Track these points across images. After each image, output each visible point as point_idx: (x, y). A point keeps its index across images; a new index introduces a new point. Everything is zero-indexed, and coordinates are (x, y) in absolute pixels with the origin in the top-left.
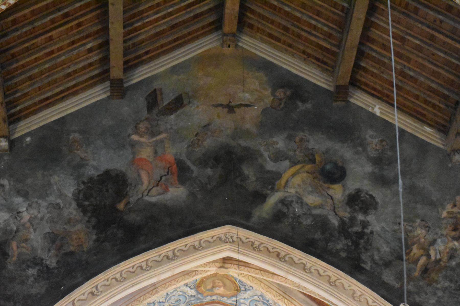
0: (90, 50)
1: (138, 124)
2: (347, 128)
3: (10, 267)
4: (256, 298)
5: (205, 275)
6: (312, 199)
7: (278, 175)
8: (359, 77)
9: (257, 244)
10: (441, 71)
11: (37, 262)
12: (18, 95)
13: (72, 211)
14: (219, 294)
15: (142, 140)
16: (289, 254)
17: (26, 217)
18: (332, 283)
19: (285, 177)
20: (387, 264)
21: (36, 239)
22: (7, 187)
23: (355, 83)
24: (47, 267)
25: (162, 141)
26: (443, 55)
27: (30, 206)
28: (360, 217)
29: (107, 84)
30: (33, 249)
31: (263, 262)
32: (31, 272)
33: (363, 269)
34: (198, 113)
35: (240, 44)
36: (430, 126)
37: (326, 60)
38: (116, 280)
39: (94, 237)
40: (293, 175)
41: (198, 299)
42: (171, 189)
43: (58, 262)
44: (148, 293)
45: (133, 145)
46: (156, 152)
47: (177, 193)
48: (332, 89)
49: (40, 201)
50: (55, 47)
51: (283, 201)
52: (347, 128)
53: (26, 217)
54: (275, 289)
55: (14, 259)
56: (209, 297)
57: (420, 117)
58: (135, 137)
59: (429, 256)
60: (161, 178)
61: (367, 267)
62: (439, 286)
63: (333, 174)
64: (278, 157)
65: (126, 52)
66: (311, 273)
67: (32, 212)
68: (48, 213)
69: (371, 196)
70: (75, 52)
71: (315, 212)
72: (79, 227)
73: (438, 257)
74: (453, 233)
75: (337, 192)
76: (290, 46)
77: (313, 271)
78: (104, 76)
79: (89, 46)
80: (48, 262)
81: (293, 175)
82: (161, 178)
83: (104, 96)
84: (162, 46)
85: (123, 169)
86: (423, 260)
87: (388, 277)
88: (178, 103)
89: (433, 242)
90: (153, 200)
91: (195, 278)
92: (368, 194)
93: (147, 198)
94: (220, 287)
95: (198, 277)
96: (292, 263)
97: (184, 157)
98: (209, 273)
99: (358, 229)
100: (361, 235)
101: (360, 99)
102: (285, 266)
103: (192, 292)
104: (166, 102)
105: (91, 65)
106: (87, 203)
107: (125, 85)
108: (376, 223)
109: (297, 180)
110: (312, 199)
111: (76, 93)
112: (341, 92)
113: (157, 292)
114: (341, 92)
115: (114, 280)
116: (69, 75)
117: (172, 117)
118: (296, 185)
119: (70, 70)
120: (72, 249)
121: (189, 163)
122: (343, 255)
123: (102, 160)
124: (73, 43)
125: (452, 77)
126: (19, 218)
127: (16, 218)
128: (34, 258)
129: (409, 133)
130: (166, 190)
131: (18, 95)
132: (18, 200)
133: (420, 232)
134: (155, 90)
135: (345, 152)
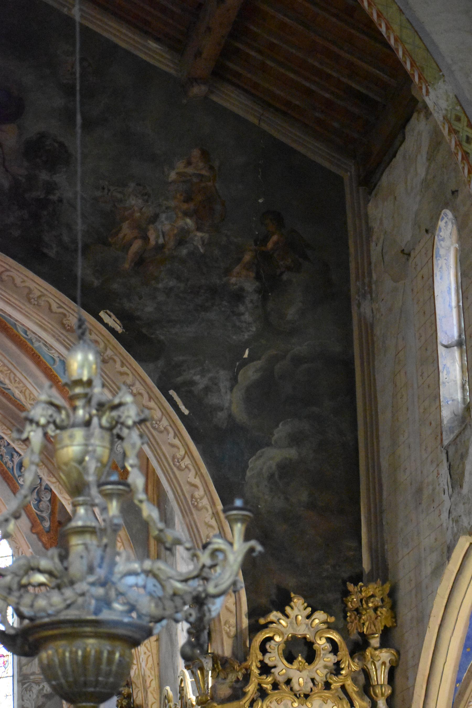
28: (44, 176)
36: (157, 40)
57: (143, 27)
59: (146, 239)
61: (52, 253)
73: (161, 241)
74: (185, 206)
86: (137, 245)
89: (154, 218)
108: (74, 189)
122: (16, 233)
133: (135, 202)
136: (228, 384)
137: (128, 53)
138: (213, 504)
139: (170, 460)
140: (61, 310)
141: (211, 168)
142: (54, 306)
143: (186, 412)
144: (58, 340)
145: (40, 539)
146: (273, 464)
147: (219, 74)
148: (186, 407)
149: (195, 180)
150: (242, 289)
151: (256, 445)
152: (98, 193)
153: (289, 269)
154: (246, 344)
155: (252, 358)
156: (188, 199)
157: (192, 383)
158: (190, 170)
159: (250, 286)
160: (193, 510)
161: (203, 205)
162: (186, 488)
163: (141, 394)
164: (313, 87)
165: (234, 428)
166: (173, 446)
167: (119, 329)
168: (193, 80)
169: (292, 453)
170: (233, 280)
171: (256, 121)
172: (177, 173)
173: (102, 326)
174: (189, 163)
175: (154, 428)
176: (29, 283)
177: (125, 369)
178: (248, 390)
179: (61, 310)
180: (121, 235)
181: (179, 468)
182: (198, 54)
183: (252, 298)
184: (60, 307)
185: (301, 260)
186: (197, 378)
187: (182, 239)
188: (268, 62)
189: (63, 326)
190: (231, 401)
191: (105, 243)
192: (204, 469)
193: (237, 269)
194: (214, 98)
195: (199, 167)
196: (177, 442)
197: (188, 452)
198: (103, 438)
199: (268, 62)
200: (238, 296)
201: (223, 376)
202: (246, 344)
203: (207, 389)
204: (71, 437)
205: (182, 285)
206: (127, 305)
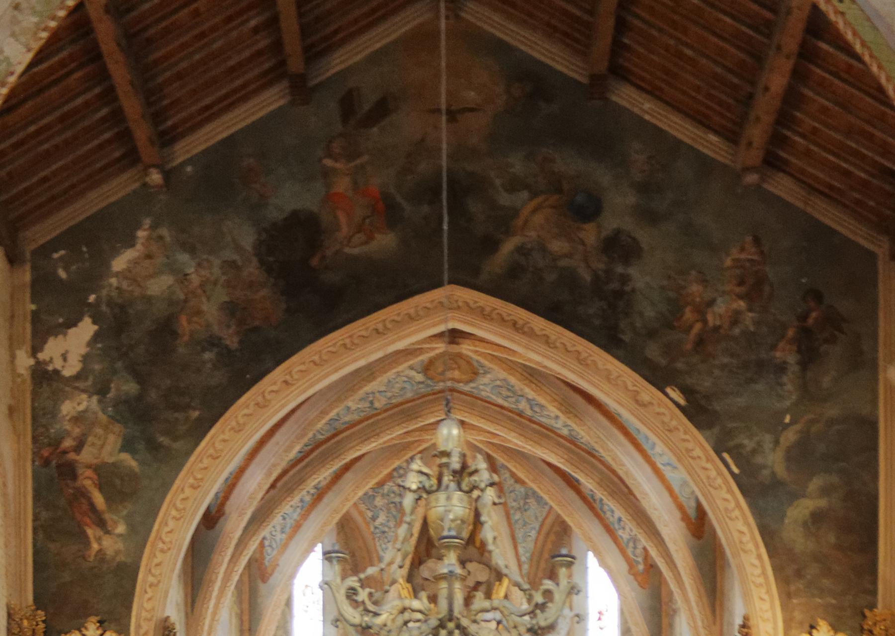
0: (256, 30)
1: (330, 142)
2: (604, 138)
3: (181, 350)
4: (498, 383)
5: (432, 354)
6: (558, 246)
7: (515, 212)
8: (621, 61)
9: (488, 309)
10: (727, 46)
11: (213, 342)
12: (165, 102)
13: (252, 270)
14: (453, 379)
15: (338, 165)
16: (528, 323)
17: (195, 280)
18: (581, 361)
19: (525, 212)
20: (652, 334)
21: (211, 310)
22: (168, 239)
23: (618, 72)
24: (227, 347)
25: (362, 166)
26: (728, 20)
27: (199, 265)
28: (620, 269)
29: (285, 84)
30: (208, 326)
31: (496, 334)
32: (207, 356)
33: (621, 340)
34: (407, 124)
35: (463, 15)
36: (716, 132)
37: (573, 33)
38: (315, 363)
39: (284, 306)
40: (535, 211)
41: (428, 386)
42: (378, 236)
43: (241, 342)
44: (363, 380)
45: (327, 174)
46: (355, 183)
47: (385, 242)
48: (584, 80)
49: (211, 258)
50: (206, 26)
51: (521, 250)
52: (604, 138)
53: (195, 280)
54: (519, 370)
55: (186, 338)
56: (442, 384)
58: (328, 162)
59: (705, 322)
60: (364, 219)
62: (717, 362)
63: (585, 208)
64: (514, 185)
65: (305, 31)
66: (556, 347)
67: (203, 273)
68: (223, 274)
69: (634, 239)
70: (235, 34)
71: (563, 263)
72: (264, 292)
73: (718, 323)
74: (738, 290)
75: (590, 234)
76: (530, 15)
77: (558, 344)
78: (278, 72)
79: (253, 23)
80: (228, 342)
81: (535, 211)
82: (364, 219)
83: (282, 102)
84: (356, 21)
85: (315, 209)
86: (698, 326)
87: (653, 351)
88: (382, 109)
89: (711, 303)
90: (356, 251)
91: (420, 358)
92: (630, 237)
93: (347, 250)
94: (453, 369)
95: (425, 357)
96: (531, 334)
97: (392, 190)
98: (437, 352)
99: (614, 286)
100: (619, 294)
101: (626, 97)
102: (524, 340)
103: (420, 377)
104: (366, 107)
105: (260, 53)
106: (271, 259)
107: (312, 83)
108: (642, 278)
109: (538, 219)
110: (558, 246)
111: (245, 99)
112: (597, 85)
113: (374, 379)
114: (597, 85)
115: (312, 364)
116: (232, 69)
117: (375, 129)
118: (535, 226)
119: (232, 63)
120: (257, 323)
121: (399, 199)
122: (597, 322)
123: (289, 197)
124: (230, 19)
125: (742, 55)
126: (186, 283)
127: (182, 282)
128: (211, 336)
129: (686, 144)
130: (370, 238)
131: (165, 102)
132: (183, 257)
133: (695, 288)
134: (350, 92)
135: (602, 176)
136: (771, 446)
137: (691, 148)
138: (757, 547)
139: (723, 512)
140: (635, 388)
141: (762, 253)
142: (629, 384)
143: (736, 470)
144: (633, 414)
145: (636, 580)
146: (807, 512)
147: (772, 162)
148: (737, 465)
149: (748, 264)
150: (785, 362)
151: (794, 496)
152: (665, 283)
153: (826, 341)
154: (787, 411)
155: (793, 422)
156: (741, 283)
157: (740, 446)
158: (743, 256)
159: (792, 359)
160: (741, 553)
161: (754, 288)
162: (736, 535)
163: (699, 457)
164: (852, 169)
165: (776, 484)
166: (726, 500)
167: (682, 402)
168: (747, 169)
169: (822, 503)
170: (778, 354)
171: (800, 205)
172: (733, 260)
173: (668, 400)
174: (742, 249)
175: (710, 485)
176: (609, 367)
177: (687, 437)
178: (788, 450)
179: (635, 388)
180: (684, 318)
181: (731, 519)
182: (750, 144)
183: (794, 368)
184: (635, 386)
185: (836, 333)
186: (746, 442)
187: (735, 318)
188: (812, 147)
189: (637, 401)
190: (774, 461)
191: (672, 327)
192: (751, 520)
193: (781, 345)
194: (766, 186)
195: (750, 254)
196: (728, 496)
197: (738, 505)
198: (461, 500)
199: (812, 147)
200: (781, 368)
201: (768, 439)
202: (787, 411)
203: (754, 452)
204: (437, 500)
205: (734, 361)
206: (689, 381)
